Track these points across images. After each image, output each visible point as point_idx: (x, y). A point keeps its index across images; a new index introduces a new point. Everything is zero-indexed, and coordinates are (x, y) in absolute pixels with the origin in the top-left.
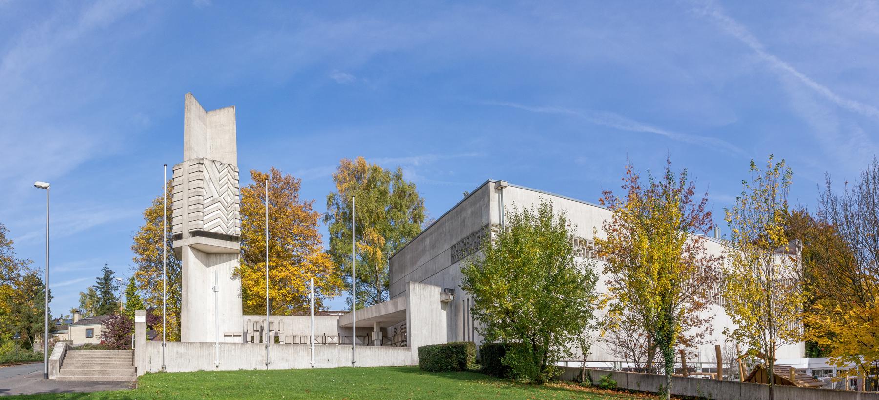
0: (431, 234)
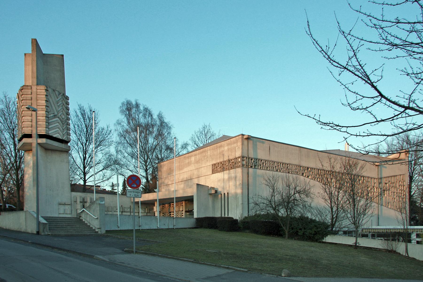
0: (195, 155)
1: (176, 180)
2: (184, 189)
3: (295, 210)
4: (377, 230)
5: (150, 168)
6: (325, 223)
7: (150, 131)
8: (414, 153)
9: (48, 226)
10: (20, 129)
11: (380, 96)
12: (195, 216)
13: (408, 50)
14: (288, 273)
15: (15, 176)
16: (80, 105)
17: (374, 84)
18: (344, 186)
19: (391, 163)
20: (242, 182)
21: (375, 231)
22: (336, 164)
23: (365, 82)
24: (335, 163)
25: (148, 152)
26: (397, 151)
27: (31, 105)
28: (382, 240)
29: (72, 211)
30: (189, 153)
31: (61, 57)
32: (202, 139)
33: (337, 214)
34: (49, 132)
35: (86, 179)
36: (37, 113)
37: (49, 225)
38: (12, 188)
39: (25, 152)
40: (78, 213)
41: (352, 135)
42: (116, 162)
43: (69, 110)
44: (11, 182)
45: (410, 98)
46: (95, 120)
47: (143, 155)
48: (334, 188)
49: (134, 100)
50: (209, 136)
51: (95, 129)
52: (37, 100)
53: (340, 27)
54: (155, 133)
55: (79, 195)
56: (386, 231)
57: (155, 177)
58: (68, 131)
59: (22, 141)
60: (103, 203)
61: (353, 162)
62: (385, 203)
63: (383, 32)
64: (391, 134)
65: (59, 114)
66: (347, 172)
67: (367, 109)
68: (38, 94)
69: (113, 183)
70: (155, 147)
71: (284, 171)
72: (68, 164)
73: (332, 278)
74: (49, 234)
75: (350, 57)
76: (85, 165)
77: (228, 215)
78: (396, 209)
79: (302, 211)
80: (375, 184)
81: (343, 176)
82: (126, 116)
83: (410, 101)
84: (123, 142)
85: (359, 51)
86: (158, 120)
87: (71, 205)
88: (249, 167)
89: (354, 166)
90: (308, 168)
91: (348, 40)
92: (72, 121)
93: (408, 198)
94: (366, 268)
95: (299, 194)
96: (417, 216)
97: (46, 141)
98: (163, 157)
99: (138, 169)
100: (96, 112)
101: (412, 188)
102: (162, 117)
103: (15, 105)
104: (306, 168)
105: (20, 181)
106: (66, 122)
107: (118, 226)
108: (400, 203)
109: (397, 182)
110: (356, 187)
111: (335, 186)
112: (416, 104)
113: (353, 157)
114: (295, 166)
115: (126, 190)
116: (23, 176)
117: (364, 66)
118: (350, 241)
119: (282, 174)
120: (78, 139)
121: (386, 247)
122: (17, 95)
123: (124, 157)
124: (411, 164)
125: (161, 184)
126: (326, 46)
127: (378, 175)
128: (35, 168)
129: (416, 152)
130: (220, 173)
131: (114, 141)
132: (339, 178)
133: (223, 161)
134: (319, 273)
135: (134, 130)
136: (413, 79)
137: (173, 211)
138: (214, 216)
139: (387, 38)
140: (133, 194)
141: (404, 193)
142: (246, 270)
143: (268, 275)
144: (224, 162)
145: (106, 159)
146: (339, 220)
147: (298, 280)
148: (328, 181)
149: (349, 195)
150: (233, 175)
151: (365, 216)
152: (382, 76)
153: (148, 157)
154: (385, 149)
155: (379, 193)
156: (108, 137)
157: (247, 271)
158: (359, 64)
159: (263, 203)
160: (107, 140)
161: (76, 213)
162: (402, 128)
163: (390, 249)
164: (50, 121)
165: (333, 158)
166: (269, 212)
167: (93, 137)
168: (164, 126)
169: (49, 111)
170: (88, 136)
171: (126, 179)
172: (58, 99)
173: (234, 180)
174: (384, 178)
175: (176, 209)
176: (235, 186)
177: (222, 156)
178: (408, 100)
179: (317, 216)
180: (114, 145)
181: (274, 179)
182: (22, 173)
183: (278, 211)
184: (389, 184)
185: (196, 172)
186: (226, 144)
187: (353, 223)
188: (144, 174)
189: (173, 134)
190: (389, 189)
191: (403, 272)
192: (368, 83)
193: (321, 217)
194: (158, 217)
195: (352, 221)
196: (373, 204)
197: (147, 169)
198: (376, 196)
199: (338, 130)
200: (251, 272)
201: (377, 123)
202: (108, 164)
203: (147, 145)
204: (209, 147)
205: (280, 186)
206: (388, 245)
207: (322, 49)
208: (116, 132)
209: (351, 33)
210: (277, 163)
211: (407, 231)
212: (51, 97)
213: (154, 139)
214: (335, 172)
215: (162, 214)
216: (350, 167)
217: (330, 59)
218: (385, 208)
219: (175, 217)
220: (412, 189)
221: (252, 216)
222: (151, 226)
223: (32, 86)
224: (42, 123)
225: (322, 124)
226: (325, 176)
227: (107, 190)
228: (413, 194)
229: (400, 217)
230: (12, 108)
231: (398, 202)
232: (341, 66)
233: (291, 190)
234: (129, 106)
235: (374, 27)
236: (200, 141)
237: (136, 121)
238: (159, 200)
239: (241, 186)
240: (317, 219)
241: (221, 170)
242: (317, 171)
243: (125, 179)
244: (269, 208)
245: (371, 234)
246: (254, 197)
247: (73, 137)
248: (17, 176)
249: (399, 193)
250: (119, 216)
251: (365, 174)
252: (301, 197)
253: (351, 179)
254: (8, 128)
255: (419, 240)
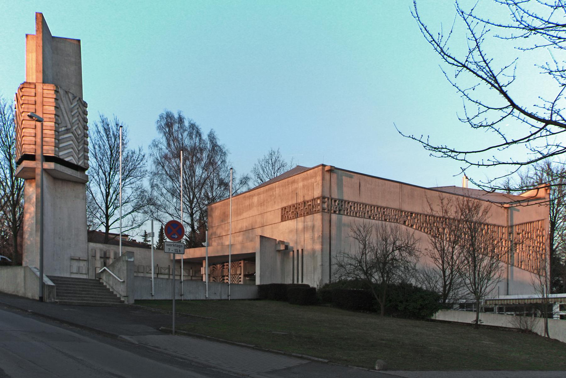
0: (259, 194)
1: (233, 230)
2: (242, 243)
3: (393, 274)
4: (506, 301)
5: (196, 211)
6: (435, 292)
7: (197, 157)
8: (558, 188)
9: (55, 291)
10: (19, 147)
11: (511, 107)
12: (258, 282)
13: (552, 36)
14: (384, 365)
15: (11, 216)
16: (103, 116)
17: (503, 88)
18: (461, 239)
19: (525, 204)
20: (322, 234)
21: (503, 303)
22: (450, 208)
23: (491, 86)
24: (449, 206)
25: (195, 188)
26: (534, 186)
27: (34, 111)
28: (512, 315)
29: (88, 270)
30: (250, 190)
31: (76, 42)
32: (268, 170)
33: (452, 279)
34: (59, 154)
35: (109, 225)
36: (42, 124)
37: (57, 289)
38: (7, 232)
39: (25, 181)
40: (97, 272)
41: (472, 164)
42: (151, 201)
43: (87, 122)
44: (5, 224)
45: (552, 108)
46: (123, 140)
47: (188, 193)
48: (447, 242)
49: (177, 112)
50: (278, 166)
51: (122, 151)
52: (43, 105)
53: (458, 4)
54: (204, 161)
55: (99, 247)
56: (519, 302)
57: (203, 224)
58: (86, 154)
59: (21, 164)
60: (132, 260)
61: (474, 203)
62: (517, 262)
63: (517, 9)
64: (526, 161)
65: (74, 128)
66: (465, 218)
67: (494, 126)
68: (44, 96)
69: (145, 232)
70: (205, 181)
71: (379, 218)
72: (84, 201)
73: (444, 372)
74: (56, 302)
75: (471, 49)
76: (108, 204)
77: (302, 282)
78: (531, 270)
79: (403, 275)
80: (504, 235)
81: (459, 225)
82: (165, 135)
83: (553, 112)
84: (160, 172)
85: (484, 39)
86: (209, 142)
87: (87, 260)
88: (332, 212)
89: (475, 209)
90: (412, 213)
91: (469, 25)
92: (91, 140)
93: (549, 254)
94: (491, 356)
95: (399, 251)
96: (560, 279)
97: (55, 166)
98: (215, 196)
99: (181, 213)
100: (124, 127)
101: (554, 239)
102: (214, 138)
103: (12, 111)
104: (409, 214)
105: (18, 222)
106: (83, 141)
107: (152, 294)
108: (537, 262)
109: (533, 231)
110: (477, 241)
111: (448, 239)
112: (561, 116)
113: (473, 196)
114: (394, 210)
115: (163, 242)
116: (22, 215)
117: (489, 62)
118: (469, 318)
119: (377, 222)
120: (99, 165)
121: (518, 326)
122: (15, 95)
123: (162, 194)
124: (553, 204)
125: (212, 234)
126: (439, 34)
127: (508, 221)
128: (39, 204)
129: (560, 186)
130: (293, 220)
131: (148, 171)
132: (454, 227)
133: (297, 204)
134: (426, 364)
135: (175, 156)
136: (557, 79)
137: (227, 274)
138: (283, 283)
139: (523, 19)
140: (173, 249)
141: (544, 246)
142: (326, 361)
143: (356, 368)
144: (298, 205)
145: (136, 196)
146: (454, 288)
147: (398, 375)
148: (439, 233)
149: (468, 252)
150: (310, 224)
151: (490, 282)
152: (514, 77)
153: (194, 196)
154: (518, 183)
155: (509, 248)
156: (141, 165)
157: (328, 362)
158: (483, 59)
159: (351, 265)
160: (139, 169)
161: (94, 273)
162: (541, 152)
163: (523, 329)
164: (61, 137)
165: (446, 199)
166: (358, 277)
167: (119, 164)
168: (217, 152)
169: (60, 122)
170: (112, 162)
171: (164, 227)
172: (72, 106)
173: (311, 231)
174: (516, 225)
175: (232, 271)
176: (313, 239)
177: (295, 196)
178: (551, 111)
179: (423, 282)
180: (149, 176)
181: (365, 229)
182: (21, 211)
183: (371, 275)
184: (522, 235)
185: (259, 219)
186: (301, 178)
187: (473, 291)
188: (189, 220)
189: (229, 162)
190: (523, 242)
191: (541, 360)
192: (495, 87)
193: (430, 284)
194: (207, 282)
195: (471, 290)
196: (501, 264)
197: (192, 212)
198: (504, 253)
199: (454, 158)
200: (333, 364)
201: (507, 145)
202: (140, 204)
203: (193, 178)
204: (277, 183)
205: (374, 239)
206: (521, 322)
207: (432, 38)
208: (151, 157)
209: (473, 14)
210: (370, 207)
211: (547, 302)
212: (62, 102)
213: (203, 170)
214: (449, 219)
215: (212, 279)
216: (469, 210)
217: (444, 53)
218: (517, 269)
219: (230, 284)
220: (555, 241)
221: (336, 283)
222: (197, 295)
223: (36, 84)
224: (50, 139)
225: (431, 149)
226: (435, 225)
227: (137, 241)
228: (556, 248)
229: (537, 282)
230: (8, 115)
231: (535, 260)
232: (458, 63)
233: (388, 245)
234: (169, 120)
235: (505, 3)
236: (266, 174)
237: (179, 143)
238: (209, 257)
239: (320, 240)
240: (424, 287)
241: (294, 216)
242: (425, 218)
243: (162, 226)
244: (358, 271)
245: (498, 308)
246: (338, 255)
247: (92, 162)
248: (14, 215)
249: (536, 247)
250: (153, 279)
251: (489, 221)
252: (402, 256)
253: (470, 228)
254: (2, 144)
255: (563, 313)
